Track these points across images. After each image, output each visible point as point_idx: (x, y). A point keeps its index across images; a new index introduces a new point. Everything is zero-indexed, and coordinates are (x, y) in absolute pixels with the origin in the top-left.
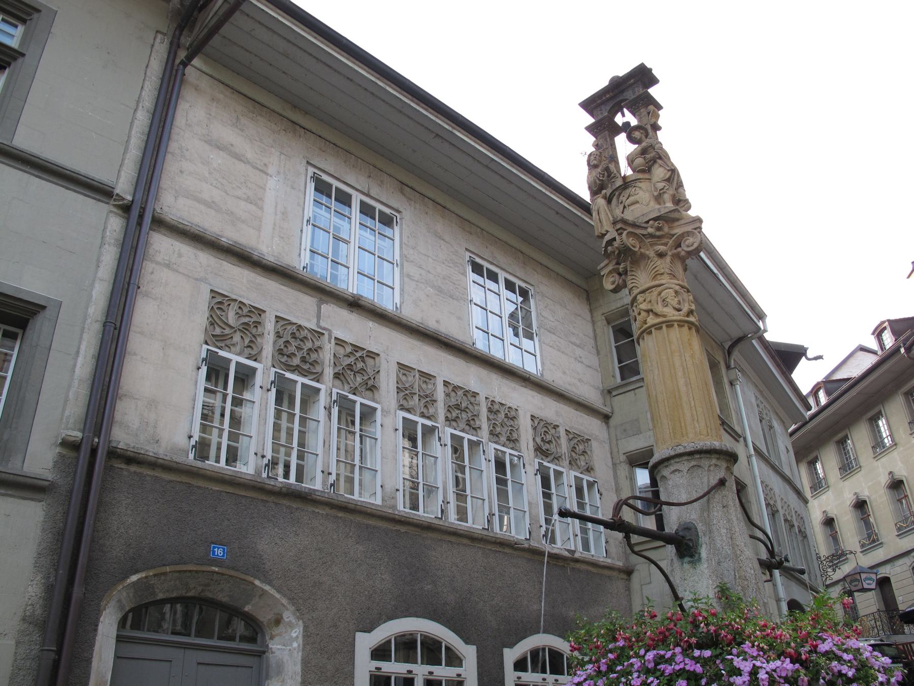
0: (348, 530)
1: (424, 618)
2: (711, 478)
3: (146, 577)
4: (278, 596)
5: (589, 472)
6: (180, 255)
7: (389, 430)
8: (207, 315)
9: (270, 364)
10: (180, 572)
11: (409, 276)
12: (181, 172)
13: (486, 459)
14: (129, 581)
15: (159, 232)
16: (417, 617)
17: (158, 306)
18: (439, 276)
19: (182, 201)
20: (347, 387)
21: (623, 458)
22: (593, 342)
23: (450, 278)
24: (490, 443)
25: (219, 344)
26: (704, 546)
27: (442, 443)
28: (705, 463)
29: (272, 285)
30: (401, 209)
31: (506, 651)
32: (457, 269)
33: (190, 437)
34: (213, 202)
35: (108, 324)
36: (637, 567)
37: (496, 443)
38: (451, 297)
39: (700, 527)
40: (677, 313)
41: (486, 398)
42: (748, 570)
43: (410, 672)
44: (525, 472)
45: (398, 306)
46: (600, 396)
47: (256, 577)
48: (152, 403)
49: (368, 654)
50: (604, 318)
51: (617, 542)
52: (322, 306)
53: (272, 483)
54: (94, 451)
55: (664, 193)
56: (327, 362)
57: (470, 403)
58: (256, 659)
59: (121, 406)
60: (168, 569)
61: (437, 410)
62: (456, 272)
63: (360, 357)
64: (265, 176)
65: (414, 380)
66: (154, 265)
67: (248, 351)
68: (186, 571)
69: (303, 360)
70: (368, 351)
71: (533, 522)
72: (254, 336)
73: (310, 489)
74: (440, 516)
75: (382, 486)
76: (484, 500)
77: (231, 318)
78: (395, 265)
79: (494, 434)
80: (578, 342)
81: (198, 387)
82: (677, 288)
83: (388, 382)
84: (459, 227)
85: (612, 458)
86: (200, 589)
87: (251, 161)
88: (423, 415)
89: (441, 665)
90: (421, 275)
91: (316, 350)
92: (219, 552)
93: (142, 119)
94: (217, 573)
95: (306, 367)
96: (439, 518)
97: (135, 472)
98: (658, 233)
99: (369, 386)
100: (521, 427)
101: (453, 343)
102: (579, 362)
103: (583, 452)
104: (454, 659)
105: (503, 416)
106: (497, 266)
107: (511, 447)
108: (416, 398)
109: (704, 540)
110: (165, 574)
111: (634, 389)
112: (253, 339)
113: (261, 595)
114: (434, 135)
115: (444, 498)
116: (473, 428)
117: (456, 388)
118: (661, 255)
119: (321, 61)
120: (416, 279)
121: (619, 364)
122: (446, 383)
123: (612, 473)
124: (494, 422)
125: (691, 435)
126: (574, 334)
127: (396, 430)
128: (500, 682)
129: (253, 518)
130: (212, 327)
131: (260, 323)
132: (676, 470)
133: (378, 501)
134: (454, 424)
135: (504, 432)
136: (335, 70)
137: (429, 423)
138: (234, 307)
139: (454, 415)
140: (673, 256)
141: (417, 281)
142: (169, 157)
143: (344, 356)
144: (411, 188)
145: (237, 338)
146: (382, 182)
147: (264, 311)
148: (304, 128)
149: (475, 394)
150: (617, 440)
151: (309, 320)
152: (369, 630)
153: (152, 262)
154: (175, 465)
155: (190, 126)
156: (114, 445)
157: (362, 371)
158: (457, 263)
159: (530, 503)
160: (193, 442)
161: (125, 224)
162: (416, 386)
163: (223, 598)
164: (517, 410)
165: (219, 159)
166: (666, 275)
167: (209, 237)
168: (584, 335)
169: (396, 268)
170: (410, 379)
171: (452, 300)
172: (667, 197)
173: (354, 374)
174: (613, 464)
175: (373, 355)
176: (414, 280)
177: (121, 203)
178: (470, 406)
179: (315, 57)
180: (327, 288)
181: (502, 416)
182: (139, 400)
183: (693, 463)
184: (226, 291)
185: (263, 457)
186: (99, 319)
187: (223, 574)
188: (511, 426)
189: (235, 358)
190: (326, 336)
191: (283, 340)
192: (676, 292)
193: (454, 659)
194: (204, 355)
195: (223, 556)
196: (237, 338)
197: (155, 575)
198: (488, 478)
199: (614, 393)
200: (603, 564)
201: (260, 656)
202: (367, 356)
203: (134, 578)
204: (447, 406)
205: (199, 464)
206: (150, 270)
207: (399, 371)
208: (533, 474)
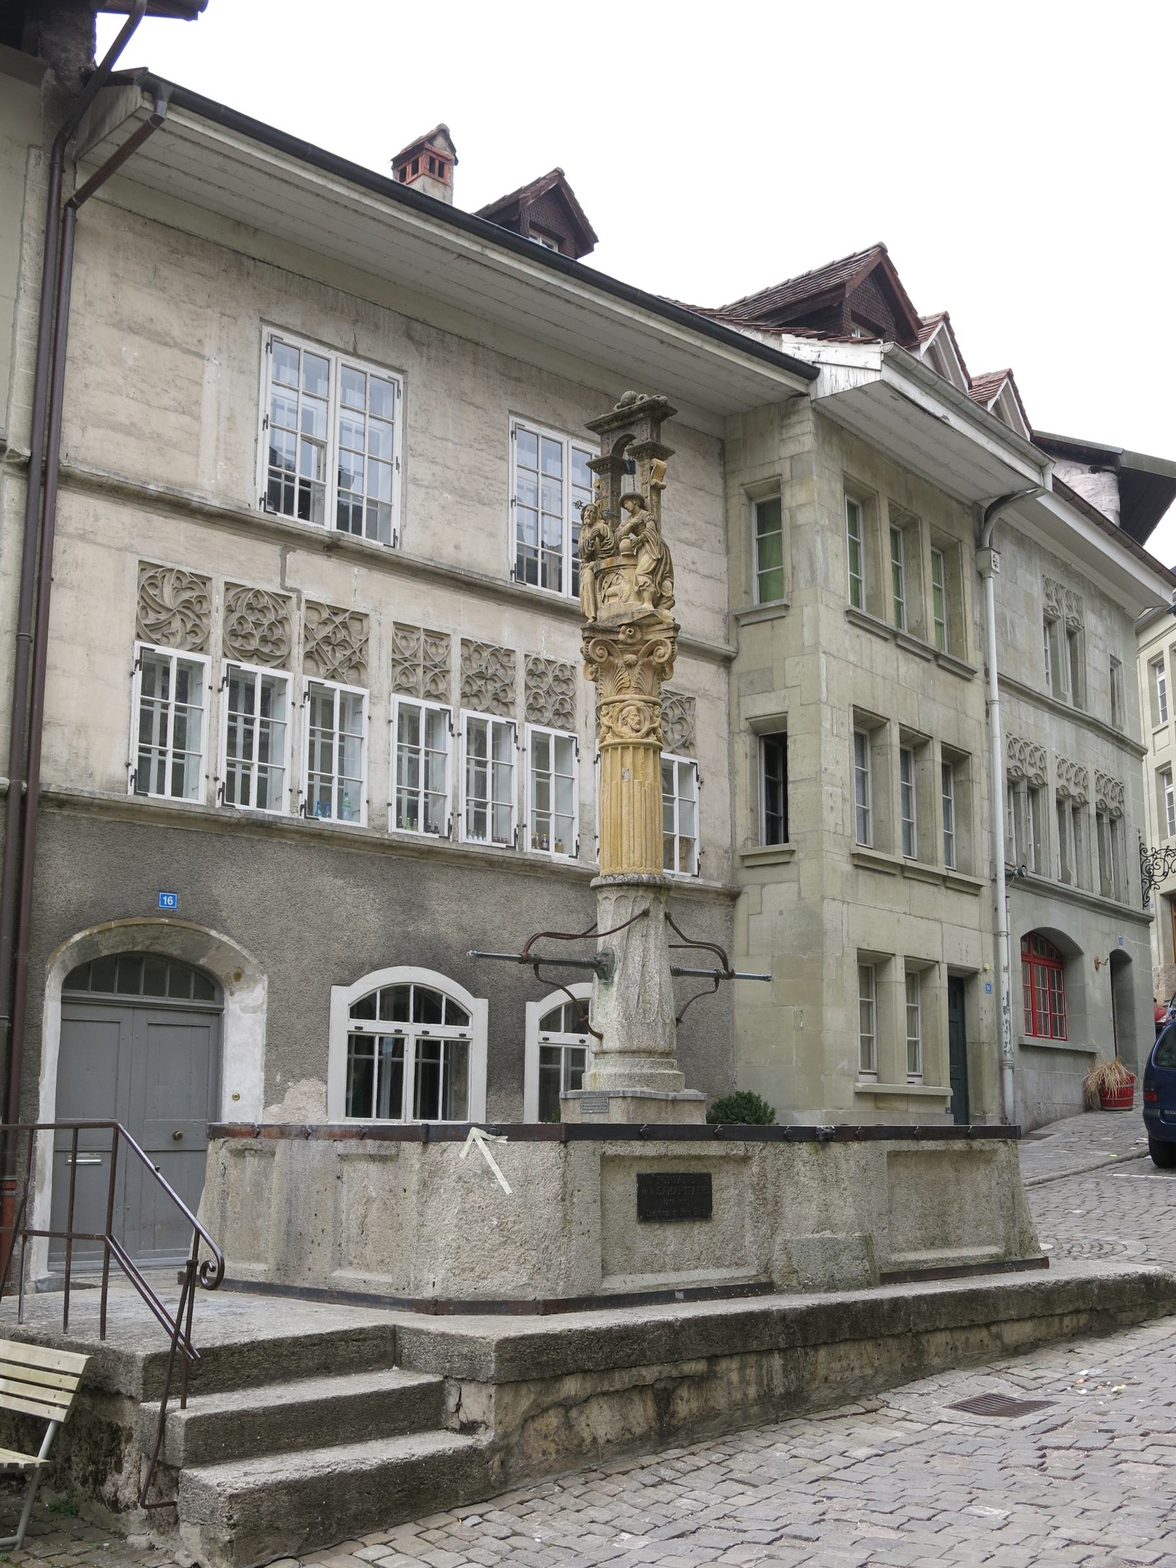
0: (324, 862)
1: (419, 966)
2: (636, 908)
3: (90, 935)
4: (237, 947)
5: (688, 747)
6: (97, 519)
7: (380, 723)
8: (137, 598)
9: (220, 653)
10: (125, 926)
11: (416, 481)
12: (86, 386)
13: (518, 748)
14: (72, 940)
15: (67, 490)
16: (410, 965)
17: (76, 597)
18: (462, 471)
19: (91, 433)
20: (322, 670)
21: (744, 725)
22: (721, 531)
23: (479, 469)
24: (526, 724)
25: (154, 637)
26: (618, 971)
27: (455, 731)
28: (632, 894)
29: (219, 538)
30: (405, 367)
31: (530, 1006)
32: (492, 450)
33: (128, 765)
34: (133, 424)
35: (22, 638)
36: (746, 889)
37: (537, 722)
38: (481, 502)
39: (618, 954)
40: (635, 734)
41: (526, 656)
42: (654, 994)
43: (398, 1031)
44: (579, 761)
45: (398, 534)
46: (722, 624)
47: (213, 927)
48: (81, 729)
49: (346, 1012)
50: (742, 491)
51: (721, 852)
52: (288, 556)
53: (228, 814)
54: (24, 799)
55: (644, 590)
56: (295, 639)
57: (502, 665)
58: (214, 1018)
59: (46, 737)
60: (113, 924)
61: (449, 685)
62: (491, 457)
63: (340, 623)
64: (199, 361)
65: (418, 644)
66: (65, 540)
67: (191, 639)
68: (132, 925)
69: (264, 640)
70: (353, 612)
71: (585, 831)
72: (198, 616)
73: (275, 816)
74: (446, 835)
75: (368, 802)
76: (511, 807)
77: (167, 595)
78: (395, 466)
79: (534, 709)
80: (692, 537)
81: (133, 700)
82: (640, 704)
83: (379, 658)
84: (502, 374)
85: (730, 724)
86: (148, 942)
87: (179, 341)
88: (429, 695)
89: (440, 1023)
90: (433, 474)
91: (280, 622)
92: (169, 900)
93: (27, 311)
94: (167, 925)
95: (266, 650)
96: (445, 838)
97: (69, 816)
98: (629, 641)
99: (353, 663)
100: (578, 693)
101: (478, 581)
102: (691, 571)
103: (680, 718)
104: (457, 1016)
105: (551, 679)
106: (561, 430)
107: (560, 724)
108: (420, 671)
109: (620, 965)
110: (110, 930)
111: (771, 620)
112: (198, 622)
113: (218, 947)
114: (456, 256)
115: (454, 808)
116: (504, 704)
117: (480, 648)
118: (630, 666)
119: (275, 177)
120: (426, 483)
121: (760, 569)
122: (465, 642)
123: (724, 746)
124: (535, 690)
125: (625, 866)
126: (688, 525)
127: (390, 722)
128: (518, 1044)
129: (207, 856)
130: (144, 611)
131: (205, 597)
132: (607, 898)
133: (363, 822)
134: (475, 700)
135: (550, 704)
136: (297, 187)
137: (436, 706)
138: (170, 580)
139: (475, 688)
140: (643, 665)
141: (427, 487)
142: (68, 364)
143: (319, 624)
144: (424, 323)
145: (176, 624)
146: (377, 326)
147: (210, 579)
148: (254, 259)
149: (509, 653)
150: (739, 696)
151: (270, 581)
152: (347, 983)
153: (63, 535)
154: (113, 804)
155: (90, 304)
156: (44, 789)
157: (344, 644)
158: (493, 440)
159: (582, 806)
160: (131, 772)
161: (24, 488)
162: (421, 653)
163: (174, 951)
164: (573, 667)
165: (133, 350)
166: (631, 689)
167: (132, 487)
168: (707, 523)
169: (395, 471)
170: (413, 644)
171: (480, 506)
172: (646, 595)
173: (333, 650)
174: (729, 733)
175: (359, 617)
176: (423, 486)
177: (17, 460)
178: (501, 672)
179: (266, 173)
180: (294, 531)
181: (549, 679)
182: (66, 726)
183: (621, 893)
184: (159, 559)
185: (216, 779)
186: (9, 629)
187: (174, 926)
188: (563, 693)
189: (175, 653)
190: (294, 600)
191: (237, 615)
192: (639, 710)
193: (457, 1016)
194: (137, 656)
195: (173, 905)
196: (176, 624)
197: (99, 932)
198: (520, 774)
199: (743, 622)
200: (690, 886)
201: (218, 1014)
202: (351, 618)
203: (77, 937)
204: (465, 676)
205: (141, 800)
206: (62, 548)
207: (396, 635)
208: (592, 762)
